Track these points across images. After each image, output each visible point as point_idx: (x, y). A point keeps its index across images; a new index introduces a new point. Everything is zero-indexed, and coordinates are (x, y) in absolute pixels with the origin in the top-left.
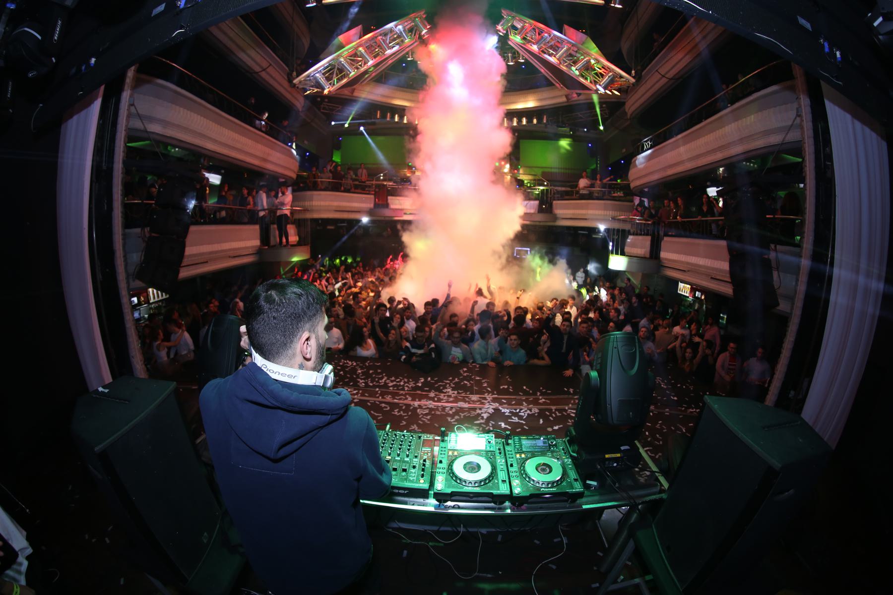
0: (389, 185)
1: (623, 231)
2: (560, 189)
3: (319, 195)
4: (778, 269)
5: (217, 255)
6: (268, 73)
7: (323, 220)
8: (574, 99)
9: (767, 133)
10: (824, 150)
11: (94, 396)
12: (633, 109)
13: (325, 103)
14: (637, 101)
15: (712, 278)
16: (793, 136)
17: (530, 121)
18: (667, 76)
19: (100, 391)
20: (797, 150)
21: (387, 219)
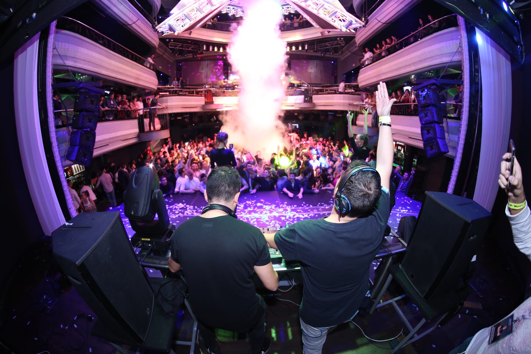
0: (213, 90)
1: (356, 112)
2: (316, 88)
3: (172, 98)
4: (448, 132)
5: (117, 139)
6: (137, 25)
7: (174, 114)
8: (326, 35)
9: (442, 55)
10: (474, 66)
11: (64, 229)
12: (360, 40)
13: (171, 43)
14: (362, 36)
15: (409, 137)
16: (456, 58)
17: (297, 48)
18: (382, 21)
19: (67, 225)
20: (459, 66)
21: (213, 110)
